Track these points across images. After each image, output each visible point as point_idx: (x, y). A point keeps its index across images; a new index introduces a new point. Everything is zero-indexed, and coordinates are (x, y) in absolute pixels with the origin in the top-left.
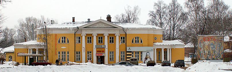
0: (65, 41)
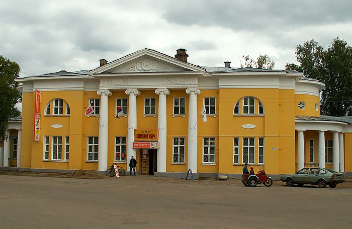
0: (61, 110)
